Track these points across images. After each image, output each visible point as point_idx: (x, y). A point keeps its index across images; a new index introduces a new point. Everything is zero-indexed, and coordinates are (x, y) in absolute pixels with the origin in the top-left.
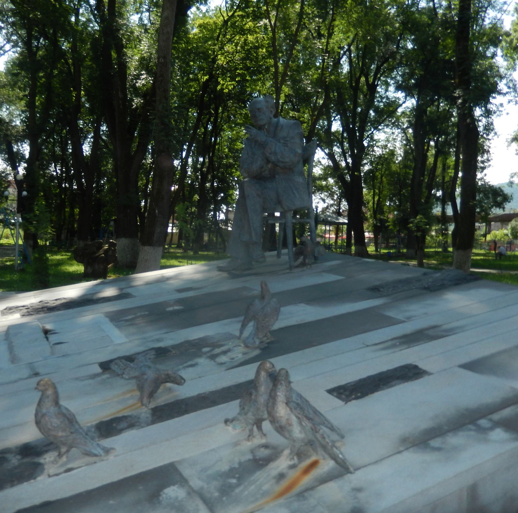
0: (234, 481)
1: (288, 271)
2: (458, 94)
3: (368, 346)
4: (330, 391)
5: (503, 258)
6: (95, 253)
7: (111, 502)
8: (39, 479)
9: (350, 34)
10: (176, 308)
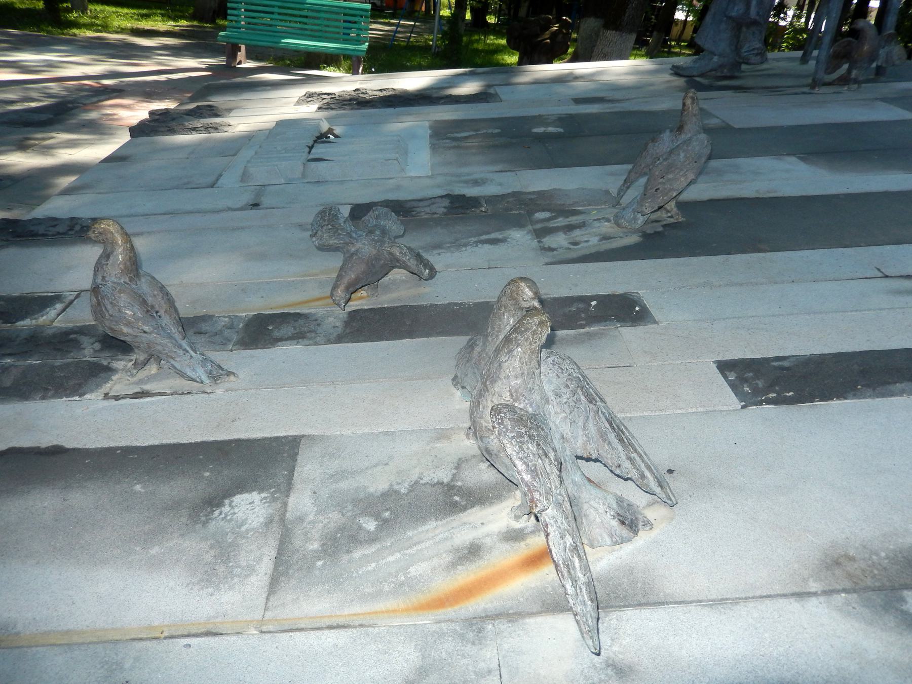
0: (370, 525)
3: (887, 276)
4: (724, 367)
6: (538, 36)
7: (138, 488)
8: (88, 396)
10: (551, 129)
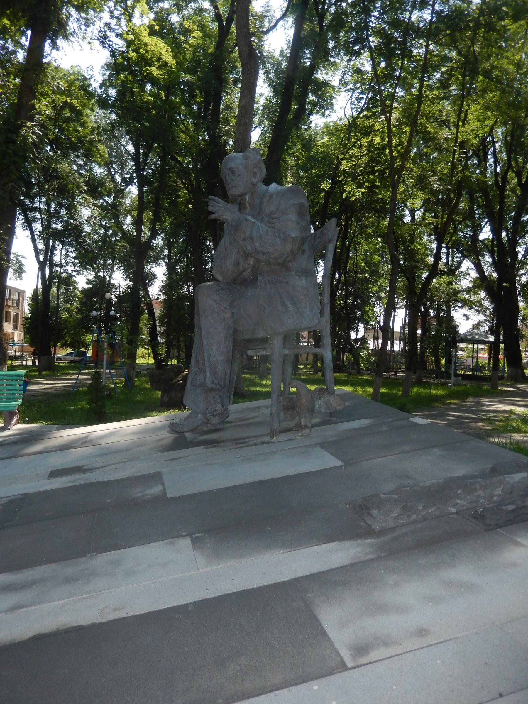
6: (173, 379)
9: (487, 122)
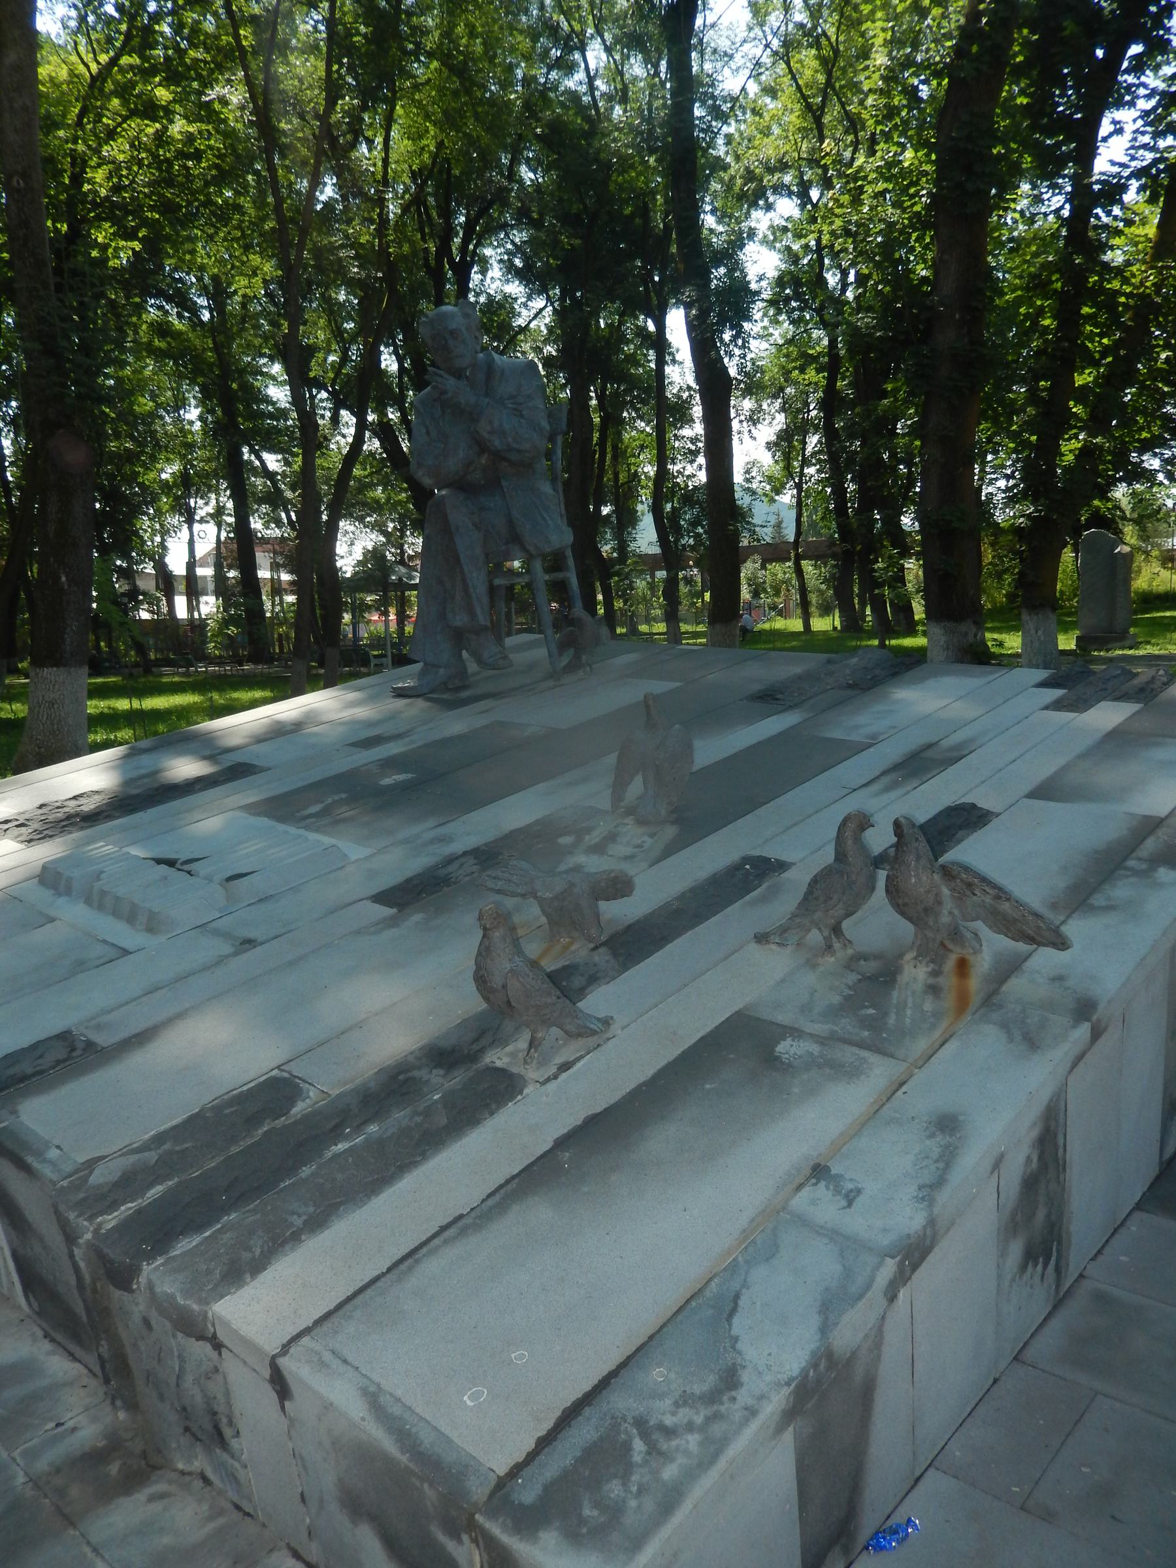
1: (551, 683)
2: (689, 296)
5: (749, 636)
